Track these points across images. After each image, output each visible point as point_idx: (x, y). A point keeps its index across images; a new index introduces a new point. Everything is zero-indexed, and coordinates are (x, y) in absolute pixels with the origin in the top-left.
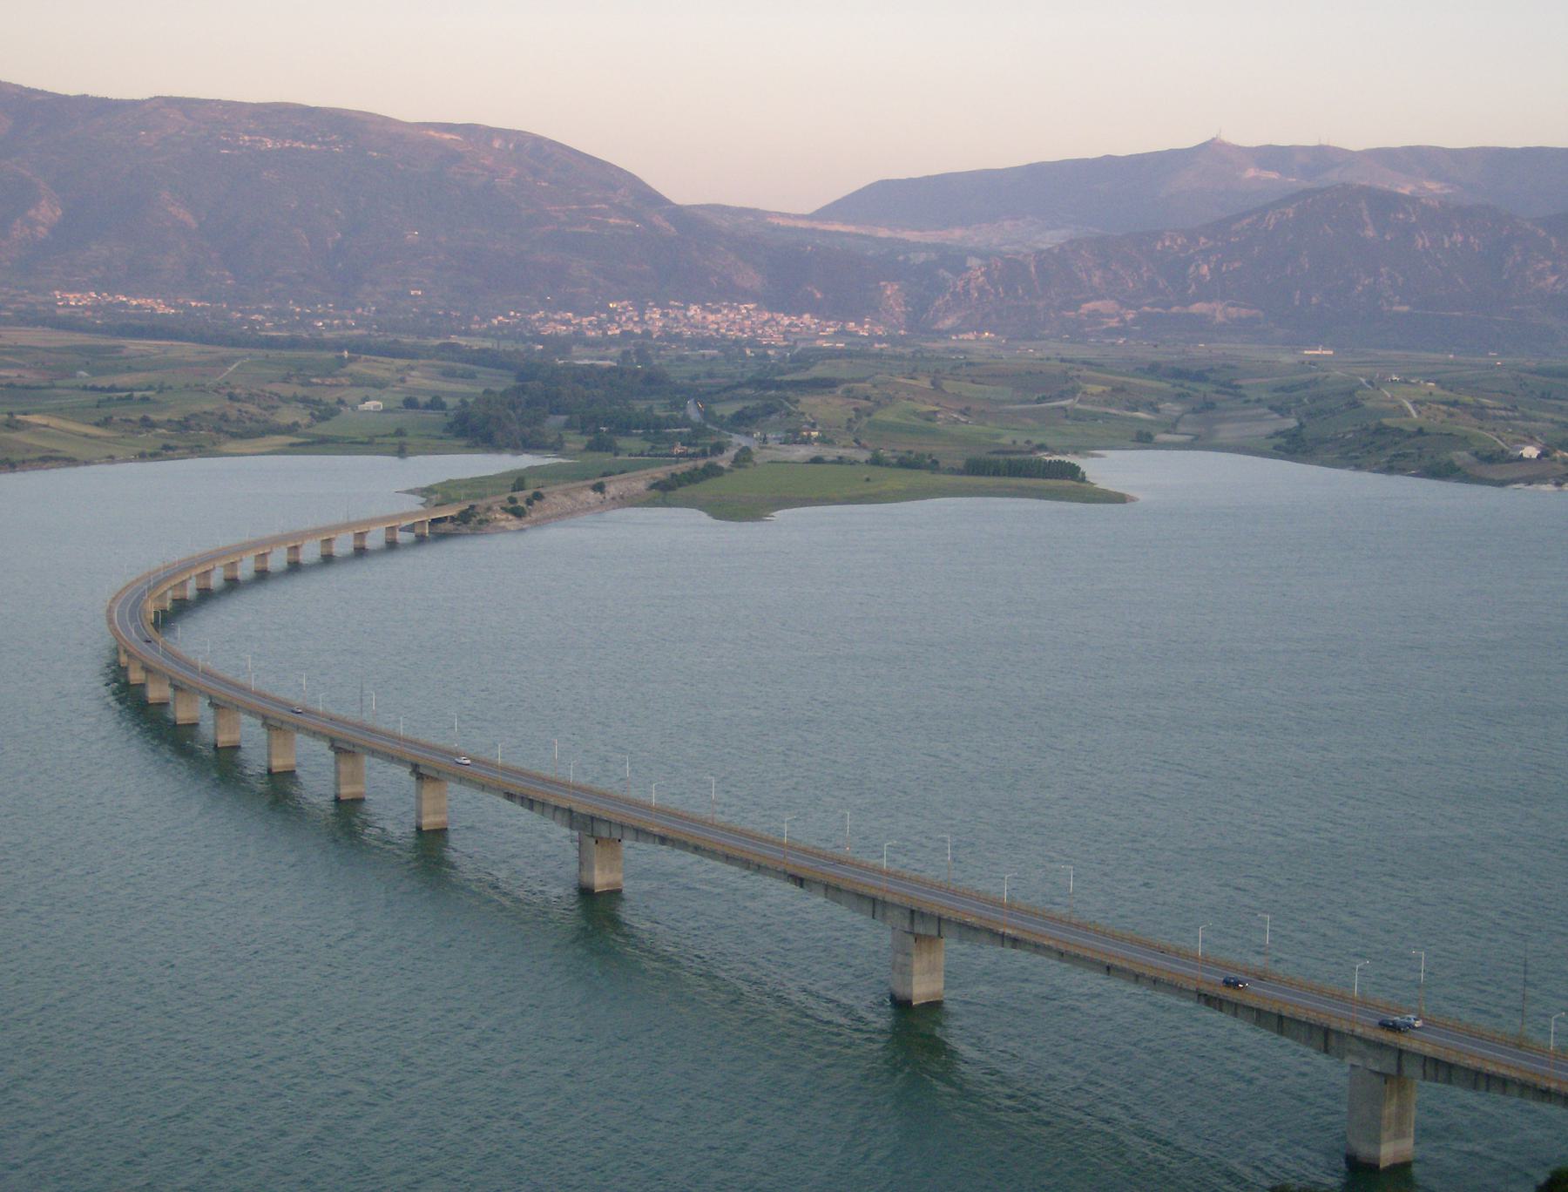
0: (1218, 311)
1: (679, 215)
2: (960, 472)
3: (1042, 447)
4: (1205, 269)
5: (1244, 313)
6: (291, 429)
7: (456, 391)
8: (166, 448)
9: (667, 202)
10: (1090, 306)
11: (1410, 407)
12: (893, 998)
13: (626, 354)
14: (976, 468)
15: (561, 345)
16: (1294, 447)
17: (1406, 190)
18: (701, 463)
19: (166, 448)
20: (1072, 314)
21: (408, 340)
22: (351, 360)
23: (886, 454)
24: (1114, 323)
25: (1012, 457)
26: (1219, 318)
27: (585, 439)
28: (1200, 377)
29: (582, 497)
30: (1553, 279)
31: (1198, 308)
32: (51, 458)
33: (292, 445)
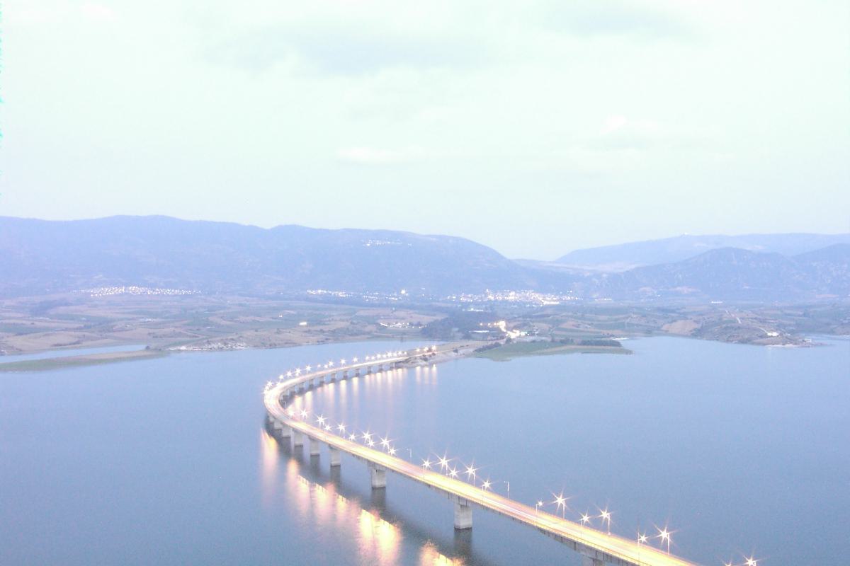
0: (684, 290)
1: (509, 260)
2: (580, 345)
3: (612, 336)
4: (680, 276)
5: (690, 290)
6: (369, 333)
7: (426, 320)
8: (327, 339)
9: (505, 258)
10: (642, 289)
11: (738, 319)
12: (455, 528)
13: (486, 308)
14: (584, 343)
15: (467, 305)
16: (698, 334)
17: (748, 249)
18: (494, 342)
19: (327, 339)
20: (636, 292)
21: (334, 306)
22: (395, 311)
23: (557, 339)
24: (650, 294)
25: (603, 339)
26: (685, 292)
27: (463, 335)
28: (673, 311)
29: (449, 354)
30: (797, 276)
31: (679, 288)
32: (605, 344)
33: (368, 338)
